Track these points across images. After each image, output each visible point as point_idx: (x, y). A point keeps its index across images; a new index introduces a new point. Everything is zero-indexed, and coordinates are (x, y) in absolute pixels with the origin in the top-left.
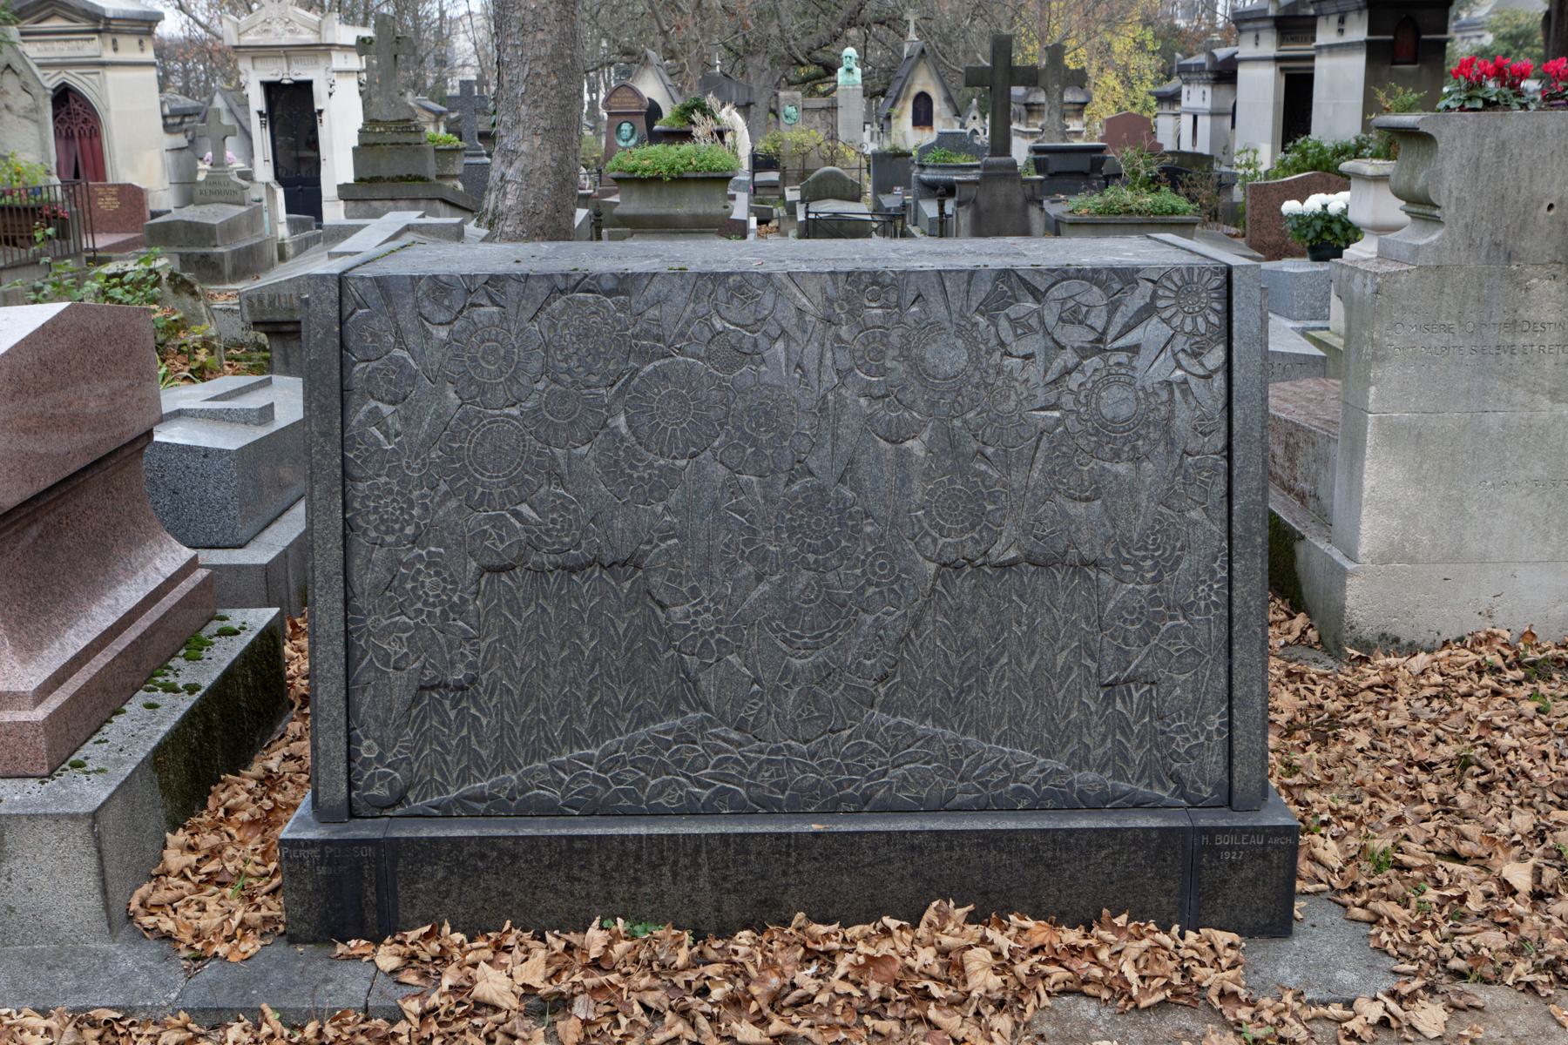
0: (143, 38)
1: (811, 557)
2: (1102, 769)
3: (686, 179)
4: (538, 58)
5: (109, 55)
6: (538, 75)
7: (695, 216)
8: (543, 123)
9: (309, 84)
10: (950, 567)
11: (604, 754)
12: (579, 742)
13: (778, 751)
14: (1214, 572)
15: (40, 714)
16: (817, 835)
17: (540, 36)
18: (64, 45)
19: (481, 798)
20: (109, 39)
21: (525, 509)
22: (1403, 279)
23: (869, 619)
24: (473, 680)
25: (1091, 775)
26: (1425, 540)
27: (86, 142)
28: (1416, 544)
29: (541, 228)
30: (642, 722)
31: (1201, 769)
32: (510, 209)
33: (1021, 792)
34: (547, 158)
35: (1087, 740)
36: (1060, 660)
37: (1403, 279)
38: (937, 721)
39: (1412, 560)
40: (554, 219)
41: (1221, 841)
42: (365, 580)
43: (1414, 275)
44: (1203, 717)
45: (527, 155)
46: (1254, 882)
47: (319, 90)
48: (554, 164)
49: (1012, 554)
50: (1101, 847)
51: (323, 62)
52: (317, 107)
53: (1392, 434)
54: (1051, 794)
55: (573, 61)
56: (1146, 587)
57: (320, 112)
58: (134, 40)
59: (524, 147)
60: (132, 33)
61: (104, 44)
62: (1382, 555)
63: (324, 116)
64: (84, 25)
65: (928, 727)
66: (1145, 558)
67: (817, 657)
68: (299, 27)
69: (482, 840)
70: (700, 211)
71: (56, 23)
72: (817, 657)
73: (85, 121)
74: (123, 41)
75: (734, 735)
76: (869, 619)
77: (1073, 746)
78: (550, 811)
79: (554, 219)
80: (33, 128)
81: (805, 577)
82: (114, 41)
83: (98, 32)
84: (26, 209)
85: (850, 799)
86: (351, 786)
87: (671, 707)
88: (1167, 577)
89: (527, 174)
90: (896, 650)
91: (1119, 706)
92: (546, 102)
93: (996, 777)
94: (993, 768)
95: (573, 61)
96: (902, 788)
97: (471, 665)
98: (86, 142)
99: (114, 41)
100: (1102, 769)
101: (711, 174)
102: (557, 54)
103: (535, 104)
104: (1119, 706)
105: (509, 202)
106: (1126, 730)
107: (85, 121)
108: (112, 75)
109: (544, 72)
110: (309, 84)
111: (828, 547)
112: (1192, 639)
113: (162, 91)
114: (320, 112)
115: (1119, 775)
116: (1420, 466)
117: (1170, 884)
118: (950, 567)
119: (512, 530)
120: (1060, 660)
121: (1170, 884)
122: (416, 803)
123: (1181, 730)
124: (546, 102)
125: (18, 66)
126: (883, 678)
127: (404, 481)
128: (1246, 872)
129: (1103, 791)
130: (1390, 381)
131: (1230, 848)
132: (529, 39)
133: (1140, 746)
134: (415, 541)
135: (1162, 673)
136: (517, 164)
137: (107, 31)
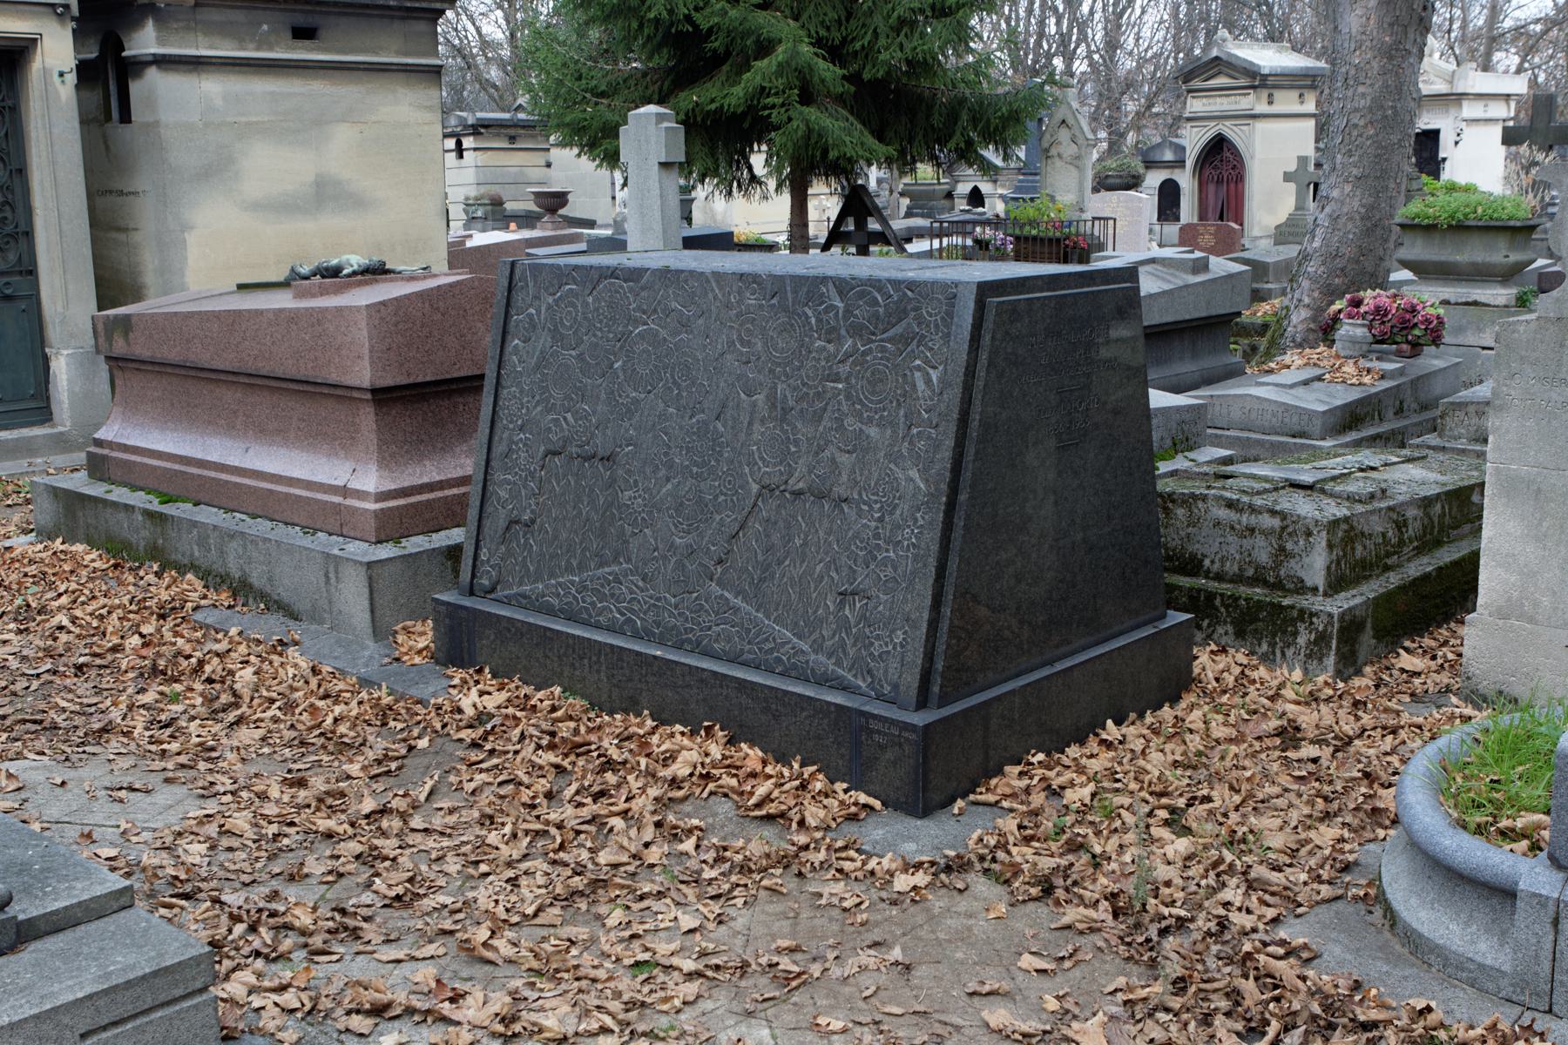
0: (1305, 92)
1: (695, 469)
2: (829, 656)
3: (1469, 228)
4: (1356, 110)
5: (1263, 108)
6: (1356, 126)
7: (1474, 264)
8: (1355, 172)
9: (1437, 132)
10: (767, 489)
11: (581, 582)
12: (572, 572)
13: (659, 599)
14: (916, 520)
15: (372, 506)
16: (655, 657)
17: (1361, 89)
18: (1225, 100)
19: (524, 596)
20: (1264, 93)
21: (569, 416)
22: (1522, 329)
23: (718, 518)
24: (533, 521)
25: (822, 658)
26: (1546, 601)
27: (1232, 186)
28: (1536, 604)
29: (1342, 270)
30: (601, 565)
31: (886, 671)
32: (1315, 251)
33: (778, 660)
34: (1356, 204)
35: (824, 633)
36: (818, 568)
37: (1522, 329)
38: (744, 599)
39: (1531, 620)
40: (1358, 262)
41: (873, 725)
42: (499, 449)
43: (1533, 325)
44: (893, 631)
45: (1336, 201)
46: (894, 763)
47: (1446, 139)
48: (1363, 210)
49: (801, 485)
50: (803, 709)
51: (1453, 111)
52: (1442, 155)
53: (1512, 487)
54: (794, 667)
55: (1396, 113)
56: (873, 524)
57: (1444, 160)
58: (1295, 94)
59: (1335, 193)
60: (1292, 87)
61: (1258, 98)
62: (1499, 609)
63: (1447, 164)
64: (1243, 82)
65: (738, 602)
66: (876, 502)
67: (689, 539)
68: (1433, 78)
69: (509, 619)
70: (1479, 260)
71: (1221, 81)
72: (689, 539)
73: (1234, 167)
74: (1278, 94)
75: (641, 584)
76: (718, 518)
77: (815, 635)
78: (550, 611)
79: (1358, 262)
80: (1074, 172)
81: (690, 482)
82: (1270, 96)
83: (1253, 87)
84: (1050, 240)
85: (689, 641)
86: (473, 576)
87: (616, 560)
88: (887, 519)
89: (1334, 219)
90: (728, 542)
91: (847, 612)
92: (1360, 151)
93: (768, 646)
94: (767, 640)
95: (1396, 113)
96: (716, 641)
97: (533, 512)
98: (1232, 186)
99: (1270, 96)
100: (829, 656)
101: (1493, 223)
102: (1377, 105)
103: (1350, 154)
104: (847, 612)
105: (1316, 244)
106: (848, 630)
107: (1234, 167)
108: (1260, 126)
109: (1362, 123)
110: (1437, 132)
111: (704, 464)
112: (895, 569)
113: (1317, 141)
114: (1444, 160)
115: (838, 663)
116: (1540, 524)
117: (843, 750)
118: (767, 489)
119: (562, 430)
120: (818, 568)
121: (843, 750)
122: (499, 594)
123: (878, 638)
124: (1360, 151)
125: (1070, 121)
126: (720, 562)
127: (521, 392)
128: (889, 755)
129: (825, 672)
130: (1508, 431)
131: (879, 732)
132: (1350, 93)
133: (854, 645)
134: (521, 429)
135: (873, 592)
136: (1327, 210)
137: (1263, 86)
